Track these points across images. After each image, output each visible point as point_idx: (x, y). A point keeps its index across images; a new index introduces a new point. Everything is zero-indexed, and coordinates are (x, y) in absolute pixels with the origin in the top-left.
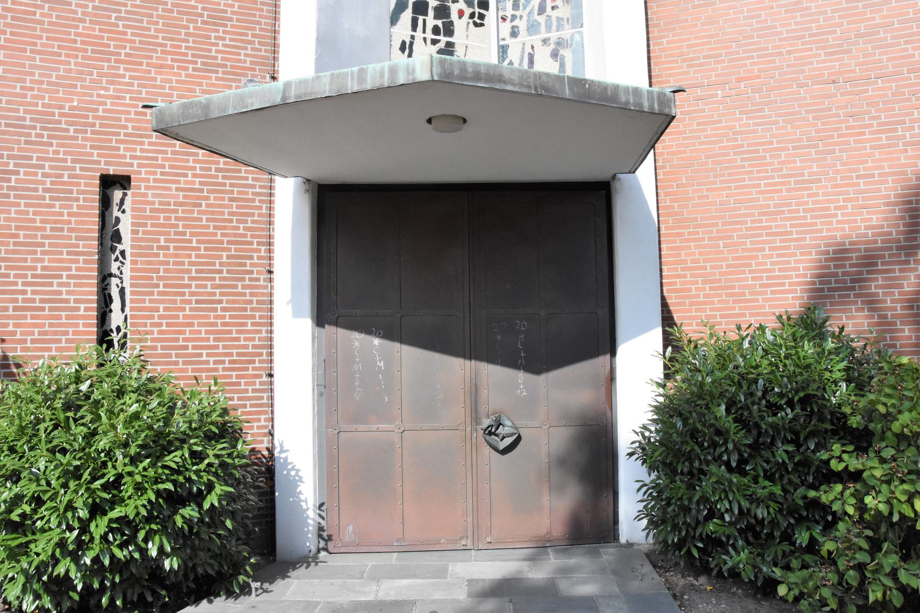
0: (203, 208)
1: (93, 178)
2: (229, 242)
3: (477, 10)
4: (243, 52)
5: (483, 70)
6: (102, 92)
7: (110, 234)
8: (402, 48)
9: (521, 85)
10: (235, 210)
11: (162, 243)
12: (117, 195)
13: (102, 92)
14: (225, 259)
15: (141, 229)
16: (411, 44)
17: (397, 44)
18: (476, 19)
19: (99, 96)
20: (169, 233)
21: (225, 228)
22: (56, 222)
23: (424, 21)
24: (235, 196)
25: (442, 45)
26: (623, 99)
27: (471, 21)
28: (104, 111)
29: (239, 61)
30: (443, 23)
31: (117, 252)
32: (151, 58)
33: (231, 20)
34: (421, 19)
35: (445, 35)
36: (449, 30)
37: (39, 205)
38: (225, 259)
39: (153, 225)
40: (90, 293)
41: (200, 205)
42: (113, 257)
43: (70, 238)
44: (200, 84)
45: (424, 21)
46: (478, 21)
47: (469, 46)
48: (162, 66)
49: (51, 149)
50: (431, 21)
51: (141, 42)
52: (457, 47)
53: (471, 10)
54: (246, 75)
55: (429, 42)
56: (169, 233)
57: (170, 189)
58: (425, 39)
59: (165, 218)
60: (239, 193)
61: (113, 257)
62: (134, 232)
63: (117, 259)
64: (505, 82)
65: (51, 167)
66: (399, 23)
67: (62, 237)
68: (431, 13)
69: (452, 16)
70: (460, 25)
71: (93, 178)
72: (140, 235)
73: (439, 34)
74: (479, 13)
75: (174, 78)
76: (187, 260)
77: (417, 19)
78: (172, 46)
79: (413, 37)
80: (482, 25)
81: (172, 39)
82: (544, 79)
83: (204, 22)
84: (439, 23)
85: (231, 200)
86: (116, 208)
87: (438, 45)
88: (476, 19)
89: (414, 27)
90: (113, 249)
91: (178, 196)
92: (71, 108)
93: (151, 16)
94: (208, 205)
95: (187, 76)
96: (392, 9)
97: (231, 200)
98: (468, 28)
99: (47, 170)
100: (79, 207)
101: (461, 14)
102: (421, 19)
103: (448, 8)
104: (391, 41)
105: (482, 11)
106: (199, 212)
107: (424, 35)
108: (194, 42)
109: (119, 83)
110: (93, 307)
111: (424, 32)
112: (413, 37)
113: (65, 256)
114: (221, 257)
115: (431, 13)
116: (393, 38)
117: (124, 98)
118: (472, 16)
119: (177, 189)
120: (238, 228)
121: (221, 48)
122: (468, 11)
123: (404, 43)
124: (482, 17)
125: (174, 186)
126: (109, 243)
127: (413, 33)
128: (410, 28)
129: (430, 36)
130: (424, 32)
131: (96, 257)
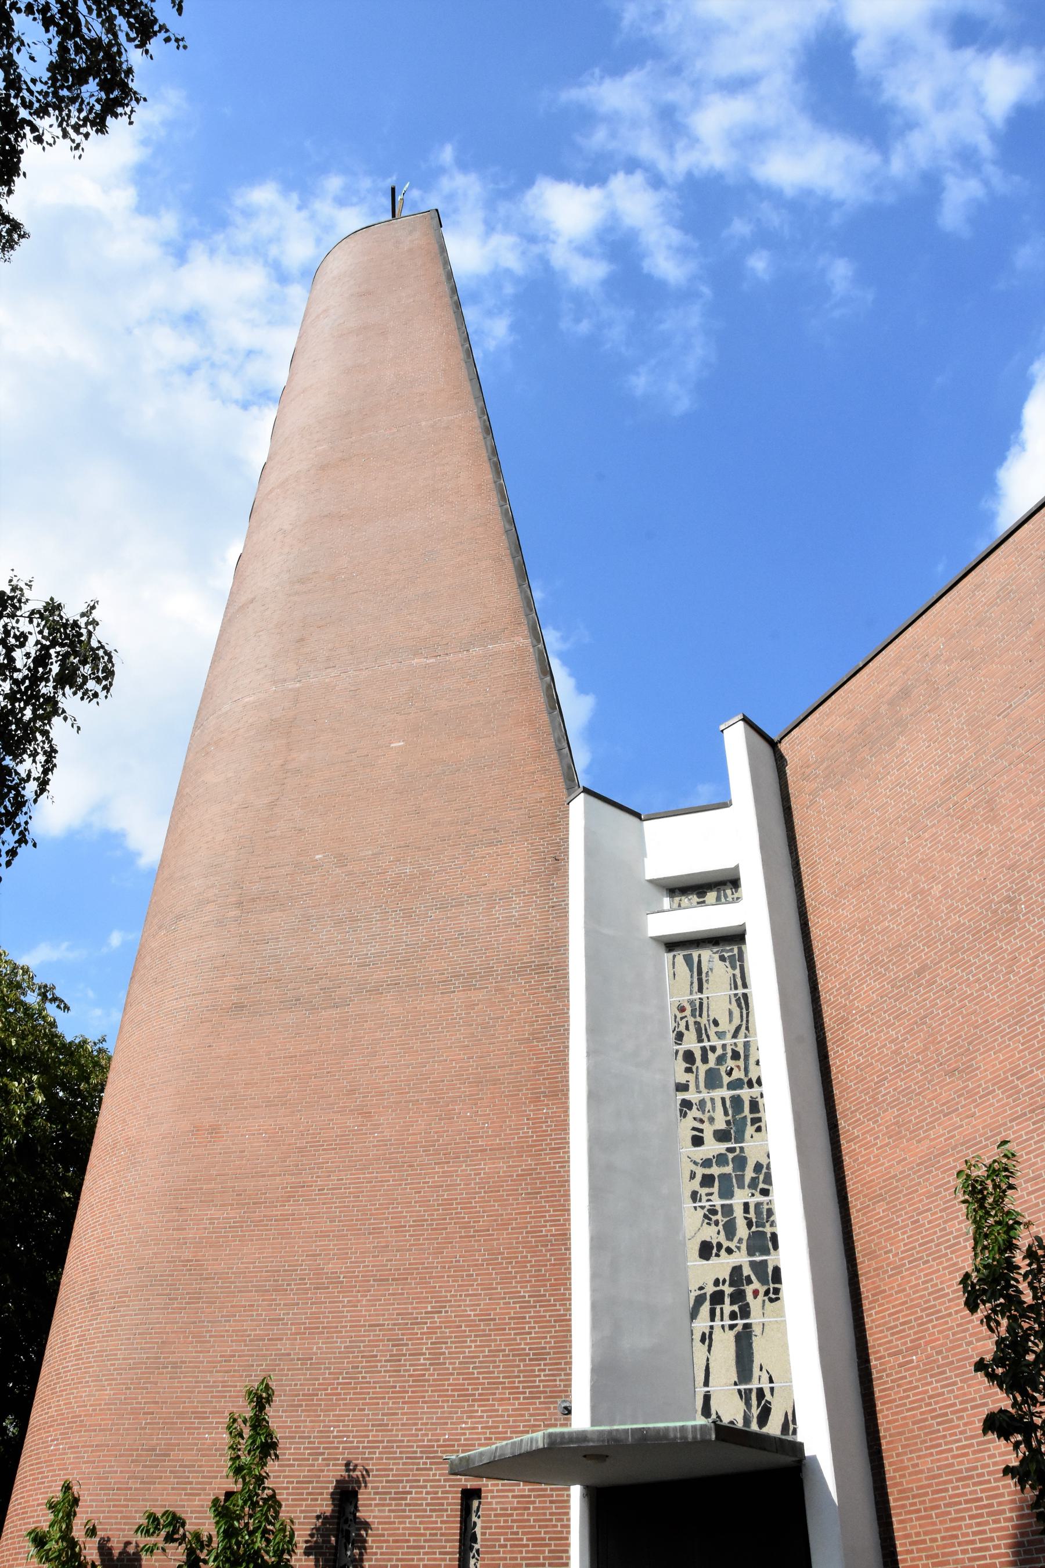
0: (531, 1510)
1: (456, 1492)
2: (550, 1539)
3: (772, 1286)
4: (558, 1378)
5: (589, 1436)
6: (464, 1426)
7: (469, 1536)
8: (703, 1340)
9: (598, 1441)
10: (554, 1511)
11: (502, 1542)
12: (475, 1503)
13: (464, 1426)
14: (547, 1554)
15: (488, 1531)
16: (711, 1333)
17: (697, 1337)
18: (771, 1295)
19: (462, 1428)
20: (506, 1534)
21: (546, 1526)
22: (433, 1529)
23: (722, 1309)
24: (554, 1498)
25: (739, 1328)
26: (672, 1435)
27: (766, 1298)
28: (465, 1440)
29: (556, 1386)
30: (740, 1307)
31: (474, 1551)
32: (495, 1394)
33: (549, 1354)
34: (718, 1308)
35: (742, 1318)
36: (745, 1312)
37: (423, 1517)
38: (547, 1554)
39: (496, 1528)
40: (454, 1534)
41: (529, 1508)
42: (472, 1555)
43: (547, 1053)
44: (528, 1410)
45: (722, 1309)
46: (774, 1296)
47: (766, 1324)
48: (502, 1399)
49: (431, 1473)
50: (728, 1308)
51: (489, 1383)
52: (754, 1327)
53: (765, 1288)
54: (560, 1397)
55: (727, 1328)
56: (506, 1534)
57: (507, 1497)
58: (723, 1327)
59: (506, 1521)
60: (557, 1495)
61: (472, 1555)
62: (483, 1534)
63: (474, 1557)
64: (588, 1441)
65: (431, 1487)
66: (699, 1317)
67: (560, 1157)
68: (727, 1300)
69: (747, 1298)
70: (755, 1305)
71: (456, 1492)
72: (487, 1536)
73: (736, 1319)
74: (774, 1288)
75: (510, 1408)
76: (519, 1556)
77: (715, 1309)
78: (509, 1383)
79: (712, 1327)
80: (778, 1299)
81: (509, 1377)
82: (614, 1433)
83: (530, 1360)
84: (736, 1308)
85: (551, 1502)
86: (474, 1514)
87: (736, 1329)
88: (771, 1295)
89: (713, 1318)
90: (472, 1548)
91: (512, 1503)
92: (445, 1440)
93: (495, 1362)
94: (535, 1508)
95: (519, 1404)
96: (691, 1306)
97: (551, 1502)
98: (763, 1306)
99: (429, 1489)
100: (448, 1516)
101: (756, 1293)
102: (718, 1308)
103: (744, 1291)
104: (692, 1335)
105: (776, 1286)
106: (528, 1515)
107: (722, 1323)
108: (524, 1377)
109: (475, 1417)
110: (455, 1565)
111: (722, 1320)
112: (712, 1327)
113: (438, 1556)
114: (544, 1552)
115: (727, 1300)
116: (694, 1332)
117: (477, 1428)
118: (767, 1293)
119: (513, 1497)
120: (556, 1526)
121: (543, 1378)
122: (762, 1290)
123: (704, 1334)
124: (777, 1291)
125: (510, 1494)
126: (468, 1542)
127: (712, 1324)
128: (709, 1319)
129: (728, 1322)
130: (722, 1320)
131: (458, 1556)
